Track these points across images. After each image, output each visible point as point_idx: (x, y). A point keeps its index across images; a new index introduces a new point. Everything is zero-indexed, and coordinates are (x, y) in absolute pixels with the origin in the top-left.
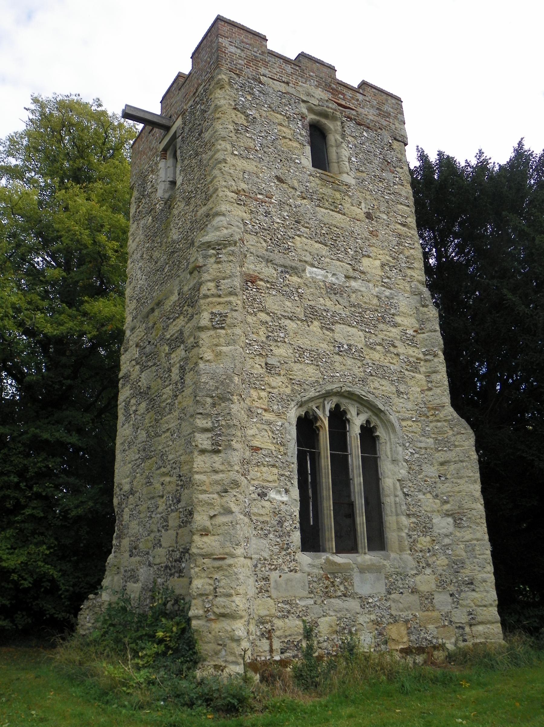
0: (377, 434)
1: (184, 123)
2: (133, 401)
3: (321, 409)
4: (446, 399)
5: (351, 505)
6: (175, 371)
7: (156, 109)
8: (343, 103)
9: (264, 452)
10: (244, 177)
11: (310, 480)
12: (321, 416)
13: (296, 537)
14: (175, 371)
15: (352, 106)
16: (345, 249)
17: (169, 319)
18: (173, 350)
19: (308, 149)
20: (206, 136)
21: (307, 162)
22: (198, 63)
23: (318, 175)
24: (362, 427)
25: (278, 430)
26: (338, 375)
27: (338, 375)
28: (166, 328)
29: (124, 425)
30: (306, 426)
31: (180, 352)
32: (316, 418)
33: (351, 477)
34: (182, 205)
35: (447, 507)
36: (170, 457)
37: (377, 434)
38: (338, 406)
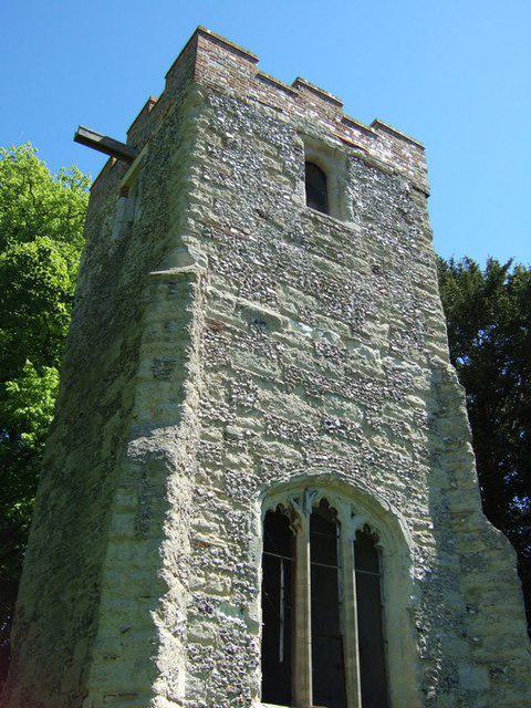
0: (380, 544)
1: (150, 152)
2: (53, 494)
3: (301, 502)
4: (476, 504)
5: (339, 640)
6: (107, 444)
7: (123, 139)
8: (348, 139)
9: (213, 551)
10: (215, 206)
11: (282, 597)
12: (299, 511)
13: (257, 677)
14: (107, 444)
15: (360, 145)
16: (343, 305)
17: (106, 381)
18: (107, 419)
19: (302, 185)
20: (173, 159)
21: (301, 196)
22: (172, 82)
23: (312, 215)
24: (358, 532)
25: (236, 523)
26: (325, 458)
27: (325, 458)
28: (102, 394)
29: (38, 526)
30: (277, 525)
31: (115, 419)
32: (294, 515)
33: (340, 600)
34: (138, 244)
35: (479, 653)
36: (88, 560)
37: (380, 544)
38: (324, 502)
